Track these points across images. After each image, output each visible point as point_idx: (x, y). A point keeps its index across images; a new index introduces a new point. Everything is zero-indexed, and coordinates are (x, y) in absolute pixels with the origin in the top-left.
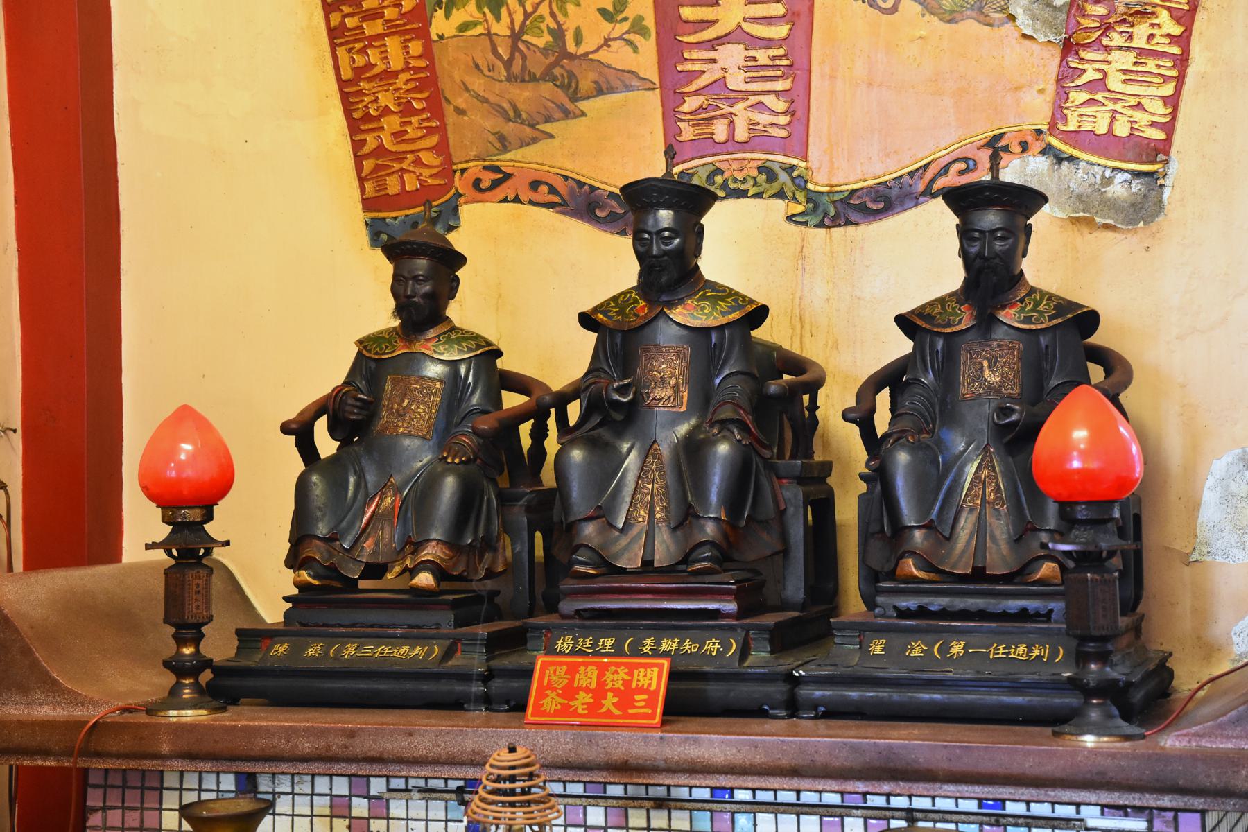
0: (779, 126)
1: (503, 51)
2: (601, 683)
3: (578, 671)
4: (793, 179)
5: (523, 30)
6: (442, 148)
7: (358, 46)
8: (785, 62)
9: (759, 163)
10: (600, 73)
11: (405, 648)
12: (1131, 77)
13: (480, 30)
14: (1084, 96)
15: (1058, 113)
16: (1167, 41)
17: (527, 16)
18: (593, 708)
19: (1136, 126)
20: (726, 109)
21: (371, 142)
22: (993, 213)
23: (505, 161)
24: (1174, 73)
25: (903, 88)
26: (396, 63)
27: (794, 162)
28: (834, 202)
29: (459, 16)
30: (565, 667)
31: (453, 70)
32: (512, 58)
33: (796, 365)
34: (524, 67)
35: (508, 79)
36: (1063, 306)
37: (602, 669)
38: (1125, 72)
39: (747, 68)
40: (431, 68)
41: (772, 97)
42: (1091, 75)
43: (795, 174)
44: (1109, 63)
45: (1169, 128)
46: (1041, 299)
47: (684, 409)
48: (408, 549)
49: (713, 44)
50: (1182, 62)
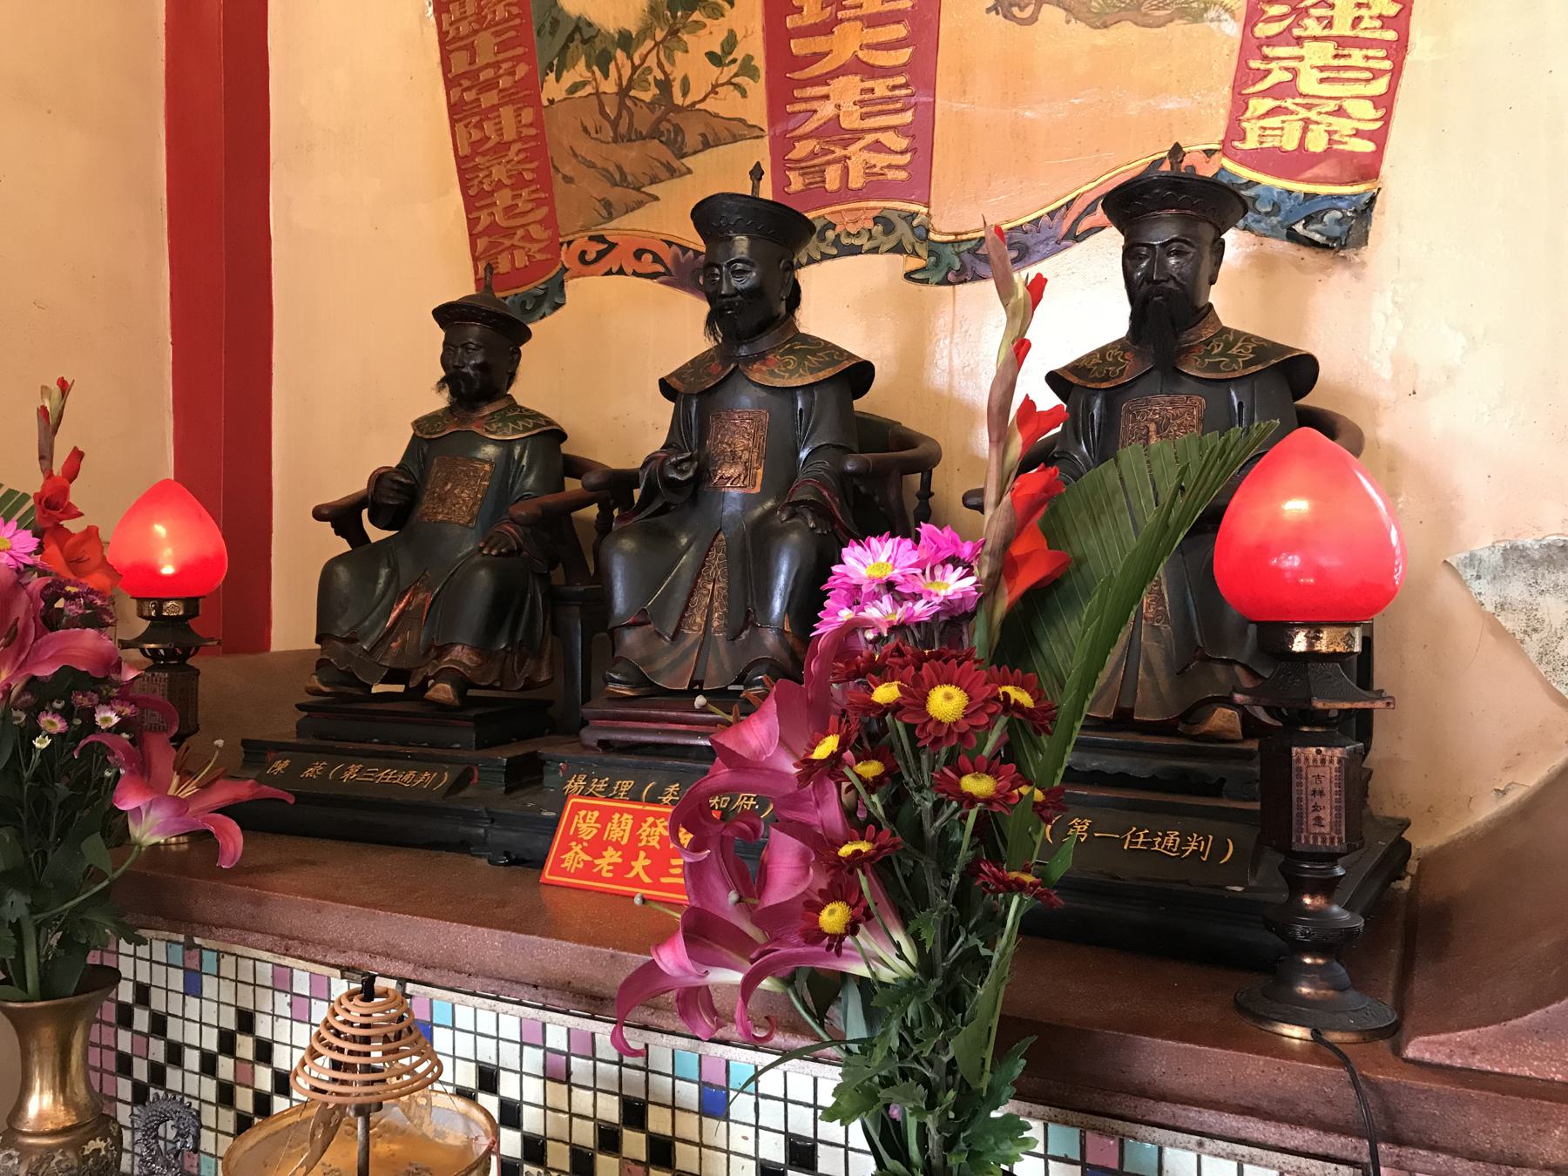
0: (898, 167)
1: (611, 111)
2: (635, 837)
3: (611, 820)
4: (913, 228)
5: (630, 86)
6: (550, 222)
7: (474, 120)
8: (904, 92)
9: (875, 213)
10: (706, 125)
11: (412, 773)
12: (1329, 74)
13: (589, 89)
14: (1269, 103)
15: (1235, 131)
16: (1378, 23)
17: (634, 68)
18: (621, 870)
19: (1336, 137)
20: (839, 152)
21: (485, 220)
22: (1168, 214)
23: (611, 229)
24: (1387, 65)
25: (1044, 110)
26: (509, 135)
27: (914, 208)
28: (958, 254)
29: (569, 78)
30: (596, 814)
31: (563, 134)
32: (619, 116)
33: (906, 440)
34: (631, 124)
35: (615, 141)
36: (1263, 349)
37: (639, 818)
38: (1321, 69)
39: (862, 103)
40: (540, 136)
41: (891, 134)
42: (1278, 76)
43: (915, 223)
44: (1301, 58)
45: (1379, 138)
46: (1236, 341)
47: (757, 489)
48: (433, 653)
49: (823, 80)
50: (1398, 51)
